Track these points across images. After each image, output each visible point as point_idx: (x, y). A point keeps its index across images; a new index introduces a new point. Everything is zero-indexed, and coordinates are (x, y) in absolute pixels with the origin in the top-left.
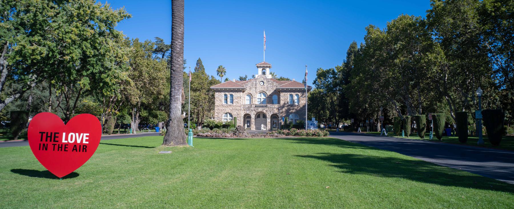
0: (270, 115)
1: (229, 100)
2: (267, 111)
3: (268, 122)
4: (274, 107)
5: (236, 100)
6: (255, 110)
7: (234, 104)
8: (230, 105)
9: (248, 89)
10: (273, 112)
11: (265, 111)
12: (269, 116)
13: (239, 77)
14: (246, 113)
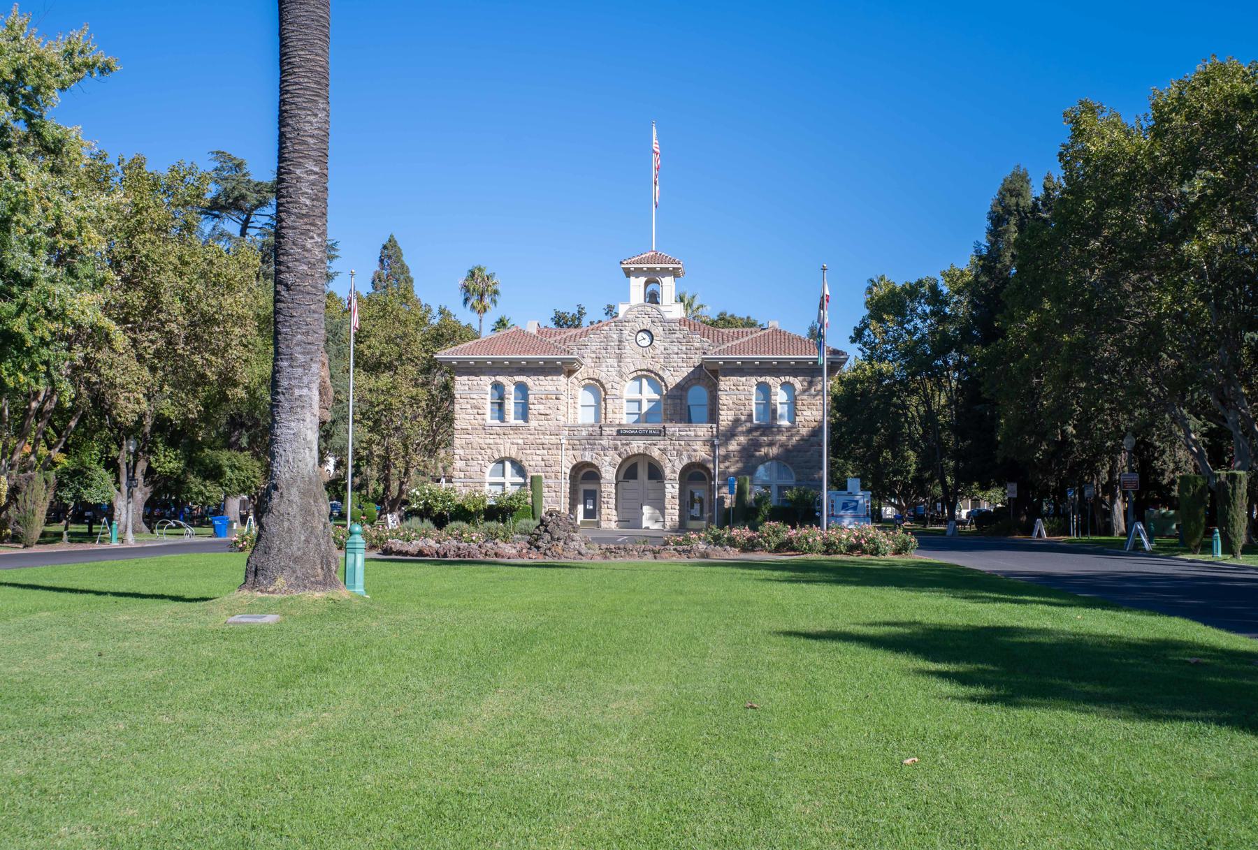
0: (679, 467)
1: (510, 406)
2: (664, 451)
3: (668, 496)
4: (692, 433)
5: (541, 407)
6: (616, 449)
10: (689, 457)
11: (656, 453)
12: (674, 472)
14: (579, 460)
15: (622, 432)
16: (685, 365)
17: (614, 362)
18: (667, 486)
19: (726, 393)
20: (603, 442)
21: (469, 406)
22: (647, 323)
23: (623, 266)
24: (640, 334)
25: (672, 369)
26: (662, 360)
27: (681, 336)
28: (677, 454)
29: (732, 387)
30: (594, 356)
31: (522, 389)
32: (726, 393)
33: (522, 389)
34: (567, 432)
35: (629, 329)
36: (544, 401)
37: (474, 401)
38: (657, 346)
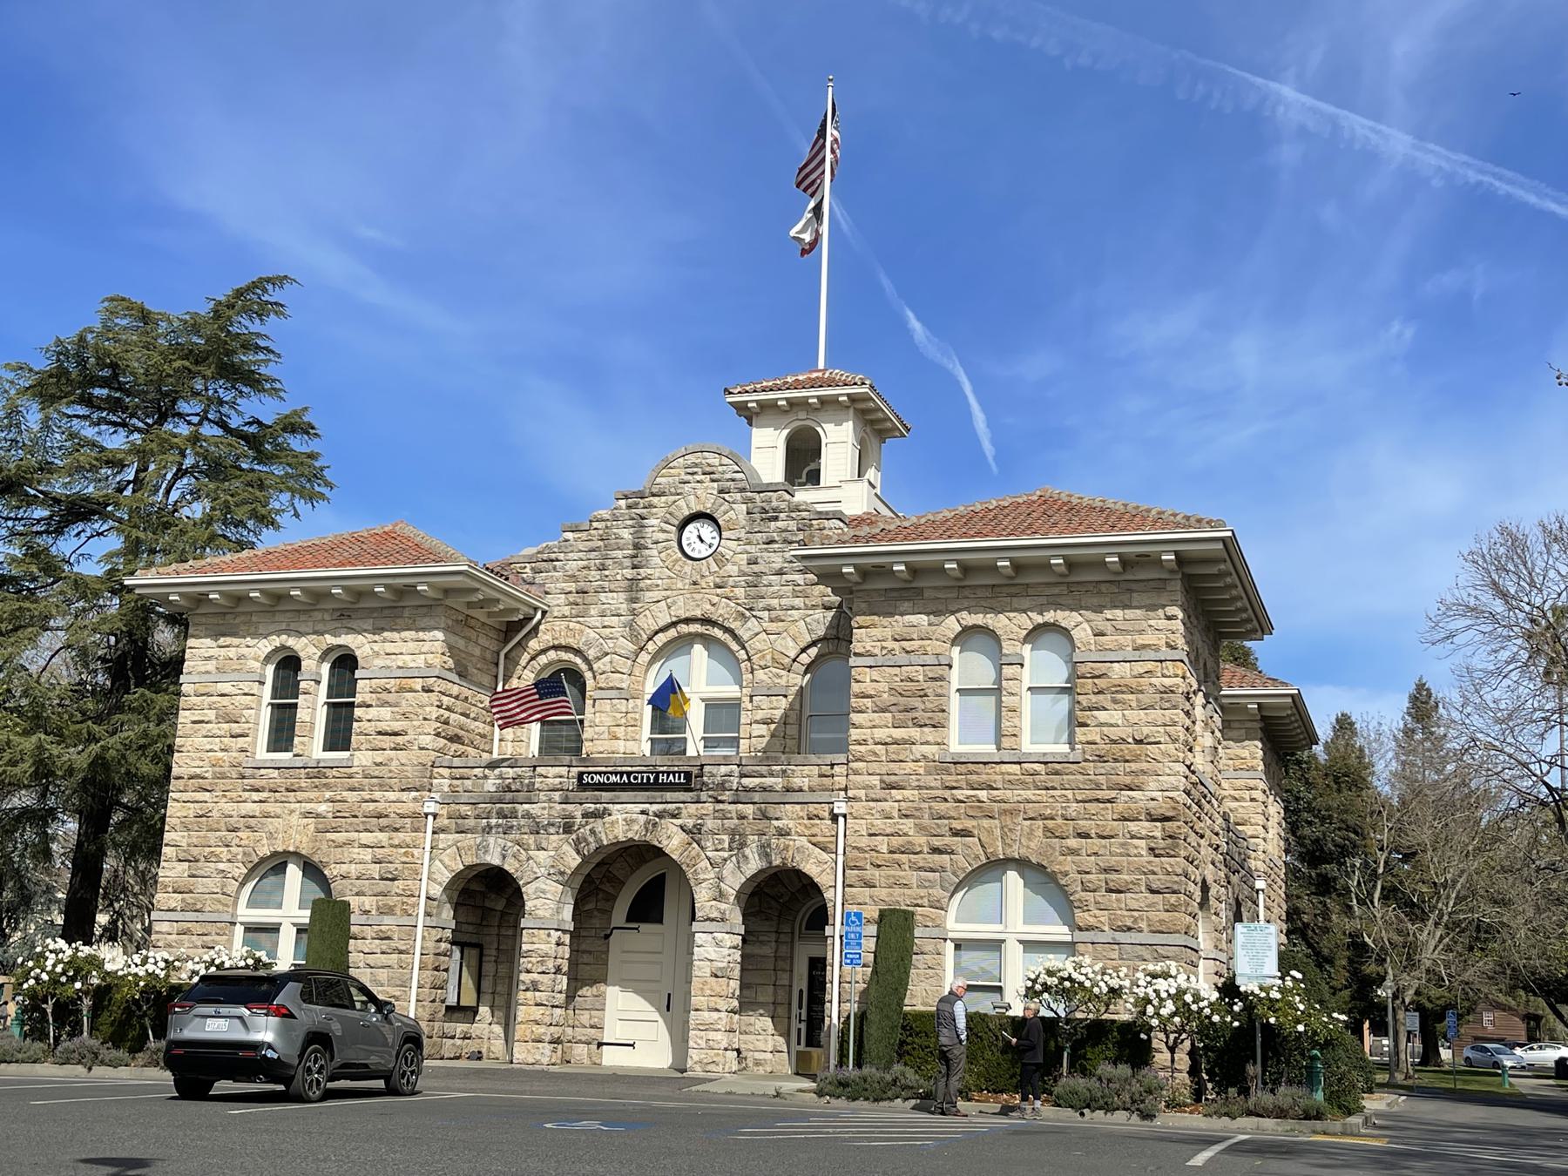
0: (734, 881)
1: (313, 710)
2: (694, 833)
3: (701, 970)
4: (777, 782)
5: (385, 712)
6: (568, 829)
7: (361, 758)
8: (318, 772)
9: (557, 603)
10: (764, 851)
11: (672, 840)
12: (720, 896)
13: (324, 448)
14: (470, 860)
15: (586, 779)
16: (798, 602)
17: (618, 601)
18: (699, 938)
19: (869, 661)
20: (534, 809)
21: (211, 715)
22: (703, 496)
23: (730, 399)
24: (690, 527)
25: (765, 614)
26: (740, 592)
27: (793, 525)
28: (732, 841)
29: (890, 644)
30: (572, 587)
31: (345, 663)
32: (869, 661)
33: (345, 663)
34: (447, 782)
35: (660, 512)
36: (391, 698)
37: (225, 701)
38: (729, 554)
